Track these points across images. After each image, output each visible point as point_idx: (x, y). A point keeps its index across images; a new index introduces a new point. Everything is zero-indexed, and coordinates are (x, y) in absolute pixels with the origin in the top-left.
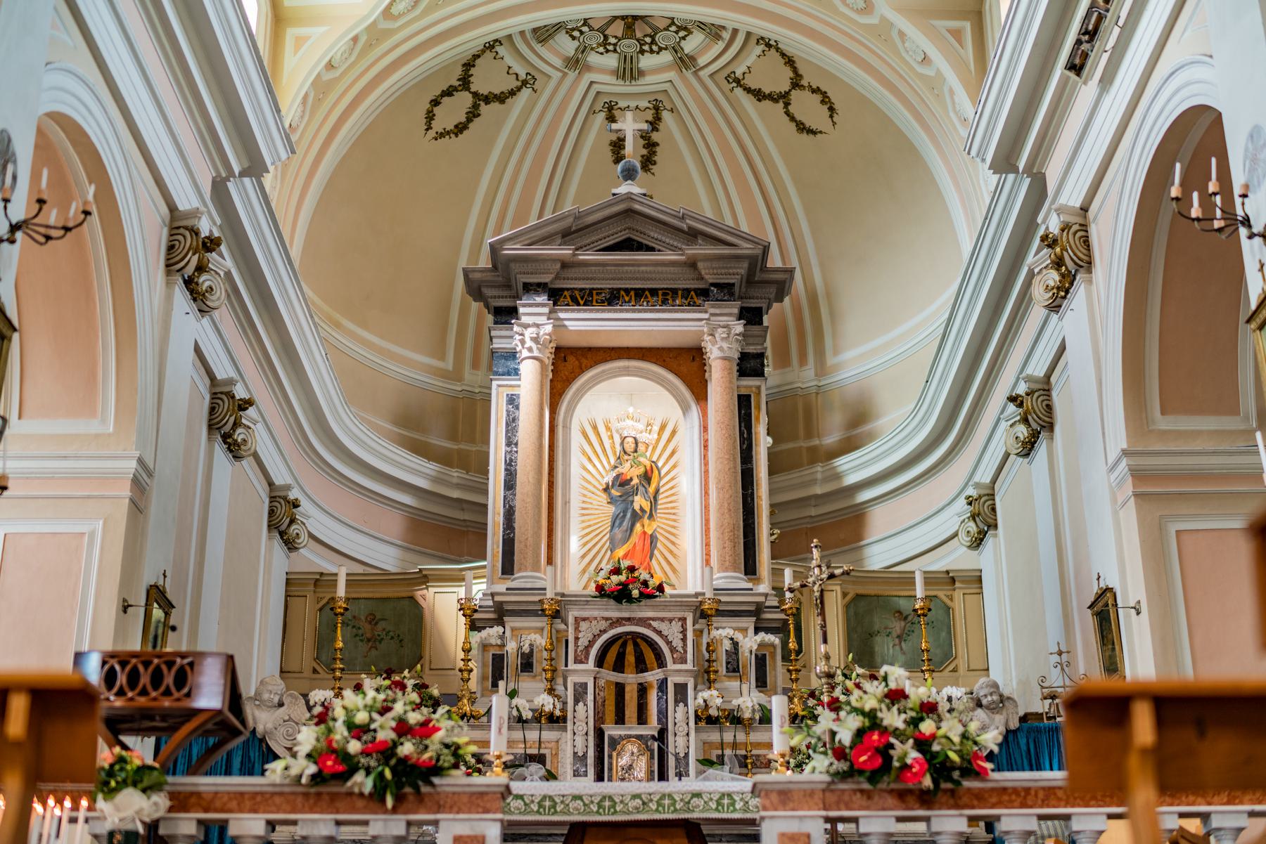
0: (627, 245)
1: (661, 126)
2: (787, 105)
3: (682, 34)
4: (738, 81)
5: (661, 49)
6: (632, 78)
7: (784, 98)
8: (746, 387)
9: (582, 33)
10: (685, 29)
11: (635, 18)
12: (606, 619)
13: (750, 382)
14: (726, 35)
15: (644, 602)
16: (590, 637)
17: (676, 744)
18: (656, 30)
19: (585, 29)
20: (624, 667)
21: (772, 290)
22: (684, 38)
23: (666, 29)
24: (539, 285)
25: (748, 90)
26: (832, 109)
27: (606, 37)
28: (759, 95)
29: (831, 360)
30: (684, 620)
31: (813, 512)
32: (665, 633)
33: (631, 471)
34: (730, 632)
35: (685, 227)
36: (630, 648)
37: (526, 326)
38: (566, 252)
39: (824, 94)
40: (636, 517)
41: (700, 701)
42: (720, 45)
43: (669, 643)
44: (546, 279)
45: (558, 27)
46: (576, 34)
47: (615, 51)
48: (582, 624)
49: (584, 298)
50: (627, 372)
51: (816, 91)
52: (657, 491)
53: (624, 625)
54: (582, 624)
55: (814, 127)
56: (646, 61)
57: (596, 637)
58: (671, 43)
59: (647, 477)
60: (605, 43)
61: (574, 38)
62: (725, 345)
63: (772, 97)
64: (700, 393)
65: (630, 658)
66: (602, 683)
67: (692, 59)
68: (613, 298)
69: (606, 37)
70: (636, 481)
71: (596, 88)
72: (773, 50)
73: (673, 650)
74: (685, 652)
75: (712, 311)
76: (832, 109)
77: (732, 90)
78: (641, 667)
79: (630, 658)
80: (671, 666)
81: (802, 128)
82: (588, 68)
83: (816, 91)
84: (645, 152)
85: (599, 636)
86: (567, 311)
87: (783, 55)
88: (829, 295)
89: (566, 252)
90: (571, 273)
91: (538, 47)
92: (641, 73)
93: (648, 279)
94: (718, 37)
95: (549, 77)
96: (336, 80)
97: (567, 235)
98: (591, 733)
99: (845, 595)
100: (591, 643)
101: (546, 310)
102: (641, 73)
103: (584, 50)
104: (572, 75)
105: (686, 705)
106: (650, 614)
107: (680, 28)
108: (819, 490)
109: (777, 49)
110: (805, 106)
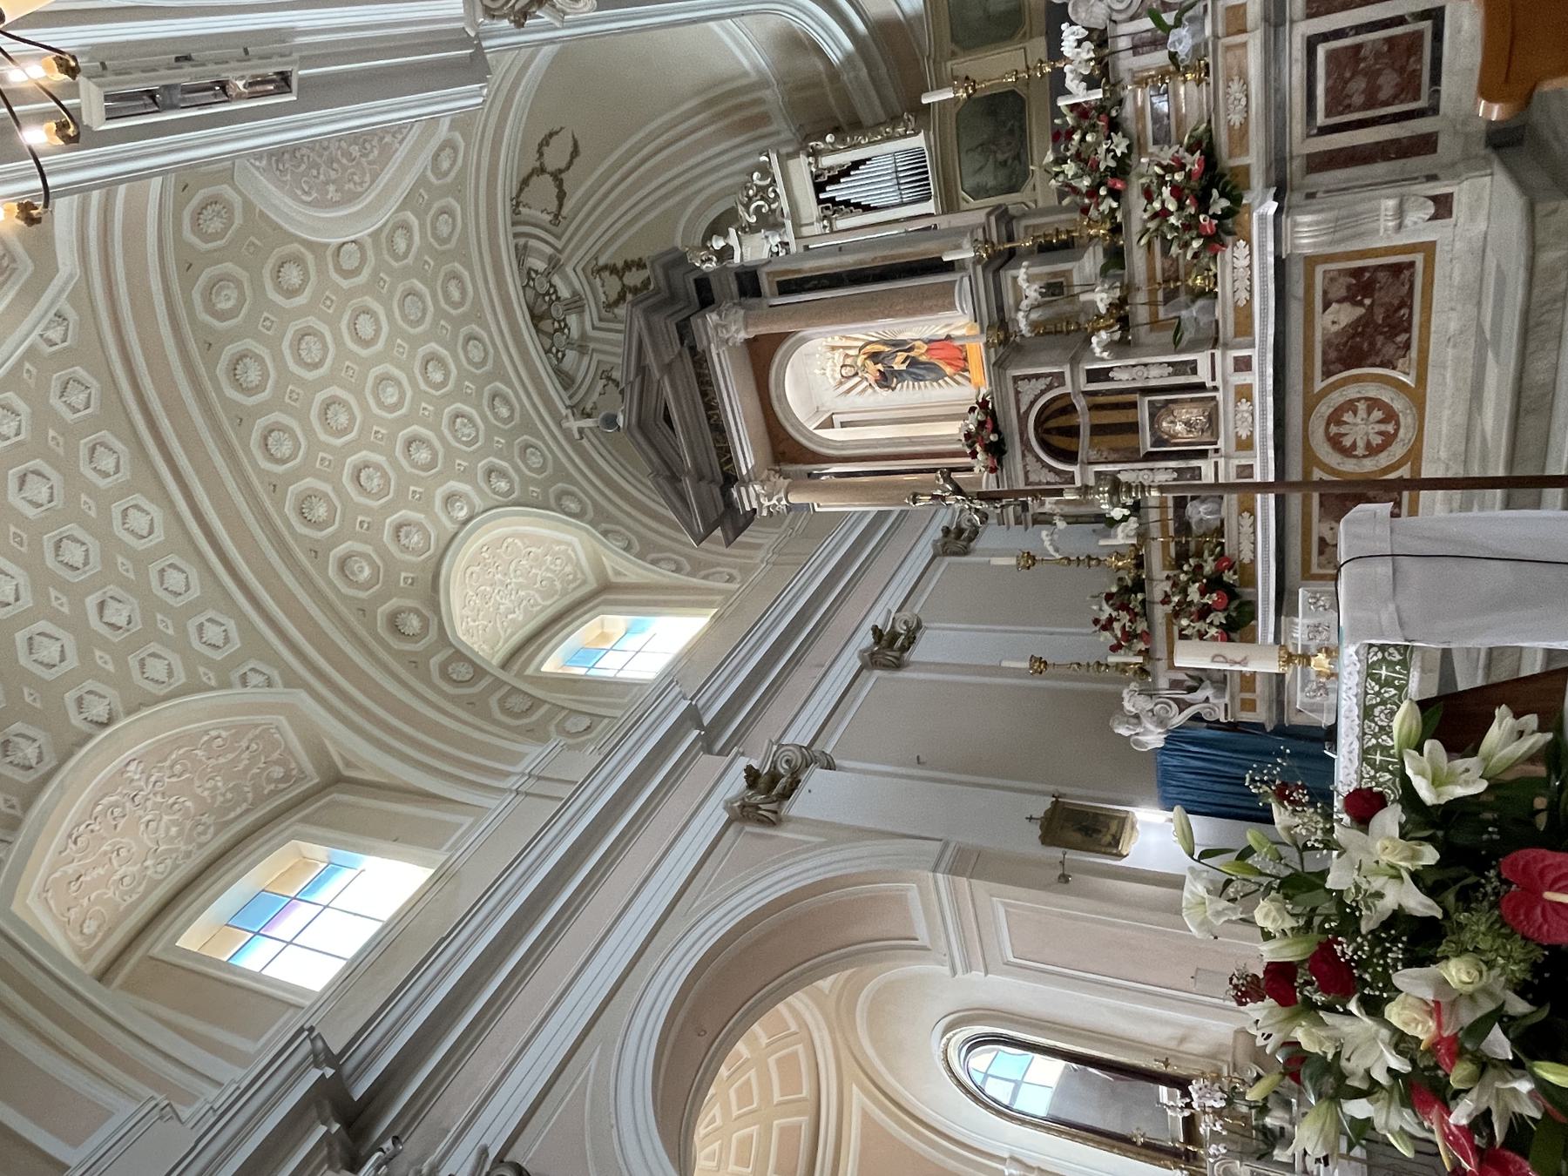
0: (668, 419)
1: (611, 262)
2: (561, 171)
3: (533, 275)
4: (556, 216)
5: (551, 285)
6: (581, 299)
7: (557, 176)
8: (770, 288)
9: (558, 351)
10: (529, 273)
11: (533, 317)
12: (1024, 456)
13: (765, 284)
14: (522, 241)
15: (1001, 428)
16: (1045, 471)
17: (1158, 377)
18: (537, 295)
19: (554, 350)
20: (1072, 427)
21: (677, 274)
22: (536, 272)
23: (534, 288)
24: (723, 495)
25: (561, 206)
26: (551, 135)
27: (556, 331)
28: (561, 196)
29: (754, 77)
30: (1016, 379)
31: (883, 70)
32: (1032, 397)
33: (873, 369)
34: (1021, 315)
35: (638, 380)
36: (1052, 424)
37: (760, 505)
38: (687, 483)
39: (541, 146)
40: (914, 362)
41: (1105, 355)
42: (533, 243)
43: (1043, 392)
44: (717, 492)
45: (558, 372)
46: (560, 355)
47: (564, 320)
48: (1031, 480)
49: (725, 453)
50: (783, 397)
51: (541, 154)
52: (885, 343)
53: (1028, 439)
54: (1031, 480)
55: (571, 144)
56: (565, 293)
57: (1045, 465)
58: (544, 280)
59: (874, 356)
60: (561, 330)
61: (564, 355)
62: (733, 328)
63: (559, 183)
64: (783, 337)
65: (1062, 421)
66: (1093, 455)
67: (551, 259)
68: (719, 429)
69: (556, 331)
70: (880, 366)
71: (597, 323)
72: (521, 199)
73: (1050, 387)
74: (1050, 374)
75: (705, 343)
76: (551, 135)
77: (564, 218)
78: (1070, 409)
79: (1062, 421)
80: (1068, 388)
81: (575, 152)
82: (584, 335)
83: (541, 154)
84: (634, 269)
85: (1042, 461)
86: (740, 469)
87: (521, 190)
88: (698, 93)
89: (687, 483)
90: (706, 470)
91: (579, 380)
92: (575, 293)
93: (694, 403)
94: (525, 246)
95: (599, 362)
96: (641, 538)
97: (674, 479)
98: (1150, 465)
99: (954, 55)
100: (1052, 469)
101: (743, 489)
102: (575, 293)
103: (570, 344)
104: (592, 345)
105: (1111, 369)
106: (1013, 413)
107: (530, 278)
108: (864, 72)
109: (518, 196)
110: (555, 157)
